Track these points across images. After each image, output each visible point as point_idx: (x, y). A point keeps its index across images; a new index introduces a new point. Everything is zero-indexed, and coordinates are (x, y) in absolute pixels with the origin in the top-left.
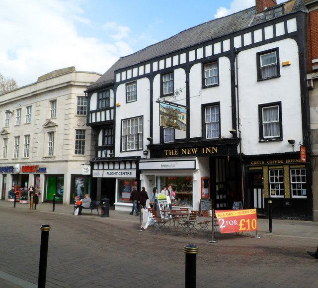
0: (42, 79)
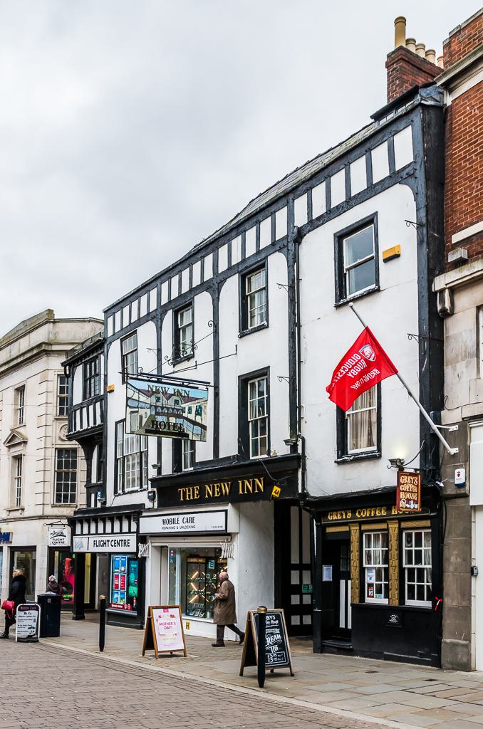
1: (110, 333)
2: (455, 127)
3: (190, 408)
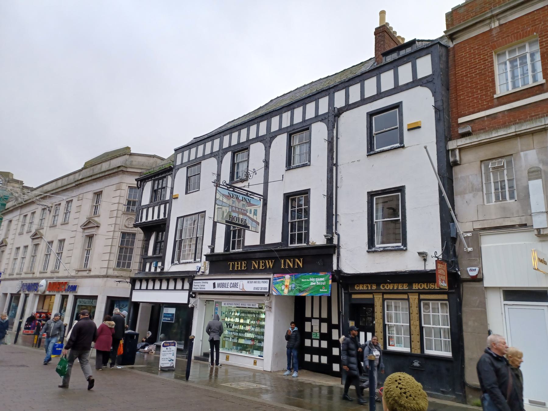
0: (89, 165)
1: (178, 162)
2: (457, 59)
3: (251, 210)
